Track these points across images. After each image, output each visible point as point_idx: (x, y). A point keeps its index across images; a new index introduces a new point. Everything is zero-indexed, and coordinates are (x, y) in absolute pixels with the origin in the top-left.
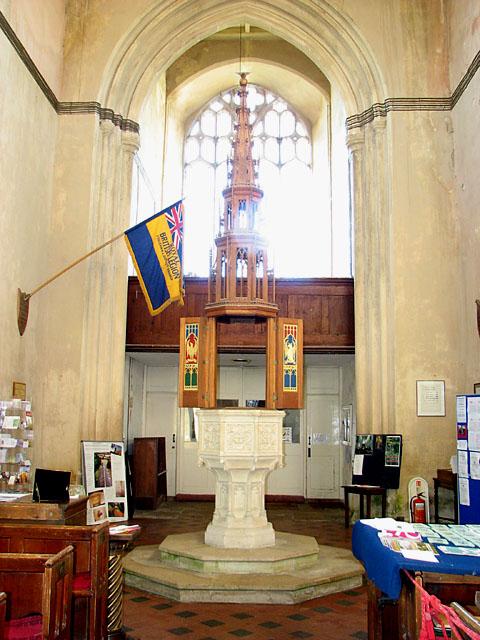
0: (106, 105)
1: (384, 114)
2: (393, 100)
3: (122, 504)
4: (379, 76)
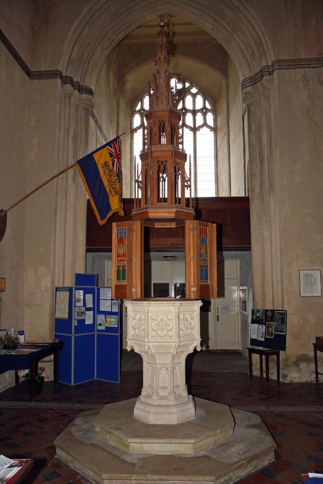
0: (66, 73)
1: (271, 73)
2: (278, 61)
3: (118, 336)
4: (268, 46)
